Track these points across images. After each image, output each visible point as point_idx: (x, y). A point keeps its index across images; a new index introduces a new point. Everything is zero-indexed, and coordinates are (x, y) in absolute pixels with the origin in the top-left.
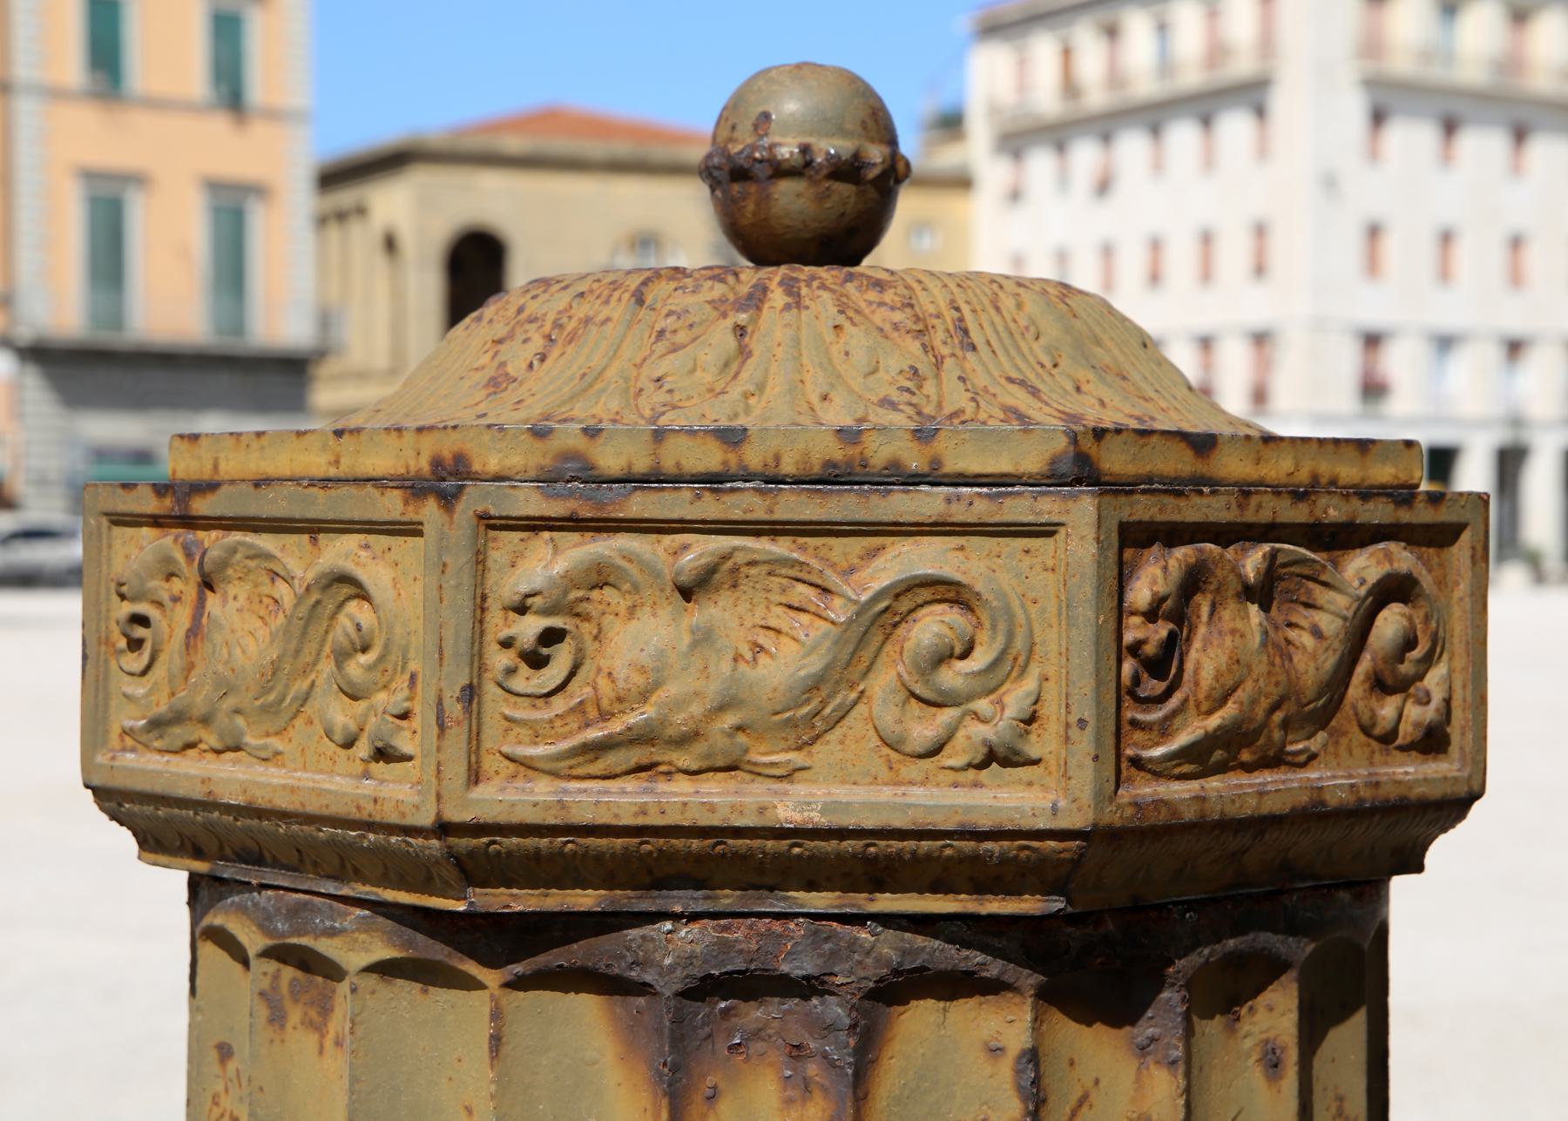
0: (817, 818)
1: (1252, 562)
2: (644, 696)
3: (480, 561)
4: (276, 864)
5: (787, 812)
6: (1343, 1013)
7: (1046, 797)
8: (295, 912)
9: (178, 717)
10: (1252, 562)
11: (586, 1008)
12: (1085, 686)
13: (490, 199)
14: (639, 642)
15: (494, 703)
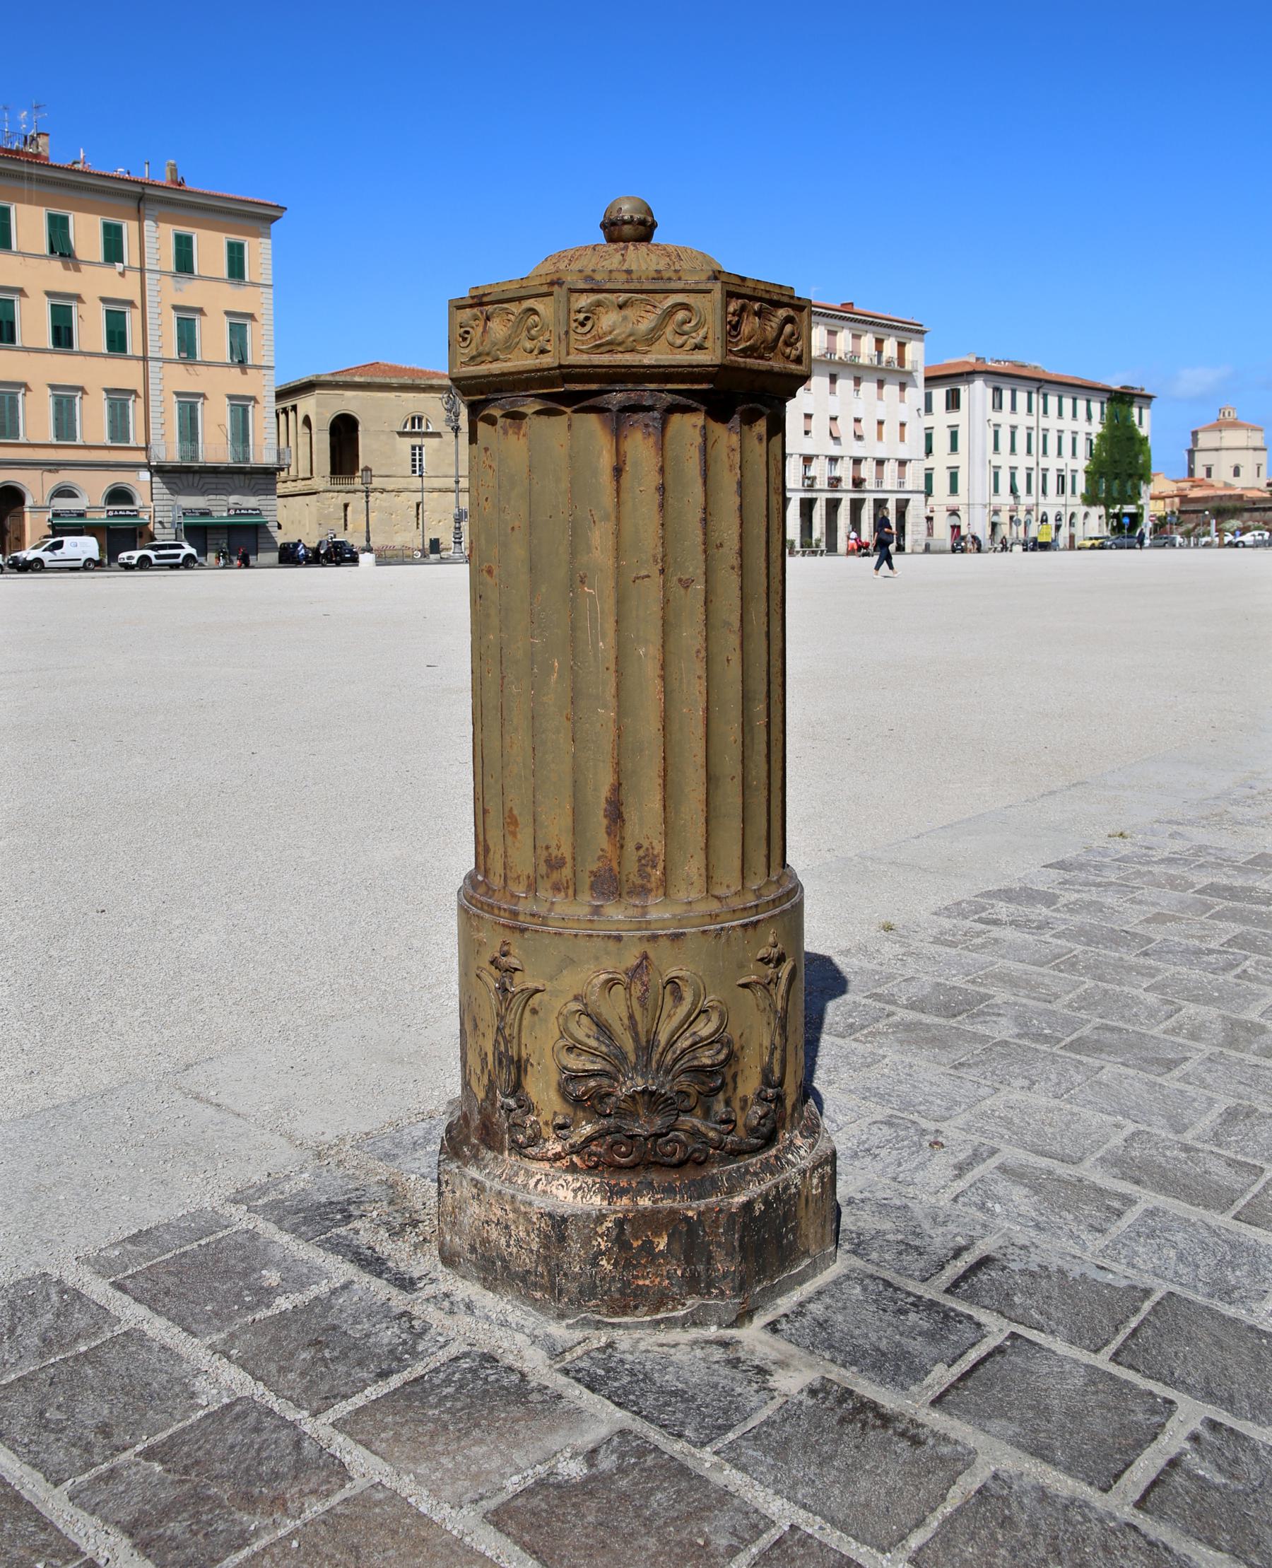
0: (653, 363)
1: (756, 306)
2: (610, 333)
3: (569, 300)
4: (506, 391)
5: (647, 360)
6: (776, 434)
7: (709, 357)
8: (512, 403)
9: (480, 355)
10: (756, 306)
11: (593, 418)
12: (719, 329)
13: (350, 402)
14: (608, 320)
15: (573, 336)
